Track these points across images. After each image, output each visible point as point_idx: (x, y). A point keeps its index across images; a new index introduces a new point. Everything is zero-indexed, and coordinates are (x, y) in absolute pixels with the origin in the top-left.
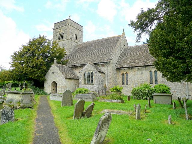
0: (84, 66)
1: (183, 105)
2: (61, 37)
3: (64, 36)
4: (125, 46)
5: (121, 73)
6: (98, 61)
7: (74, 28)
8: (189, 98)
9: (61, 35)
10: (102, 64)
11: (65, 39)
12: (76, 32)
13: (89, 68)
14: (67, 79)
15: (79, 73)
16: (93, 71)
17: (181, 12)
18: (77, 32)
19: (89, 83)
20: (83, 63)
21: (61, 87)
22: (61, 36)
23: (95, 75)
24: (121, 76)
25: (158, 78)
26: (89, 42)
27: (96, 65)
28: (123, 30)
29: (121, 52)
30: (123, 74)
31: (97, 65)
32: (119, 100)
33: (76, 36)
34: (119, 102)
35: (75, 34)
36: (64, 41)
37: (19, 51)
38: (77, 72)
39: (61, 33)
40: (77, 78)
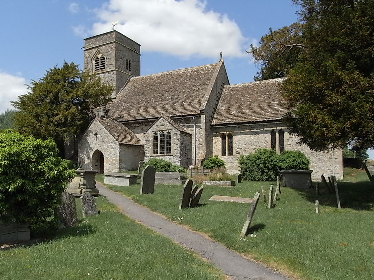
1: (274, 193)
2: (100, 63)
6: (179, 112)
7: (125, 49)
9: (100, 61)
11: (109, 70)
17: (319, 13)
19: (164, 153)
20: (150, 115)
21: (111, 160)
25: (285, 144)
28: (221, 55)
32: (229, 182)
34: (228, 184)
35: (127, 60)
37: (28, 94)
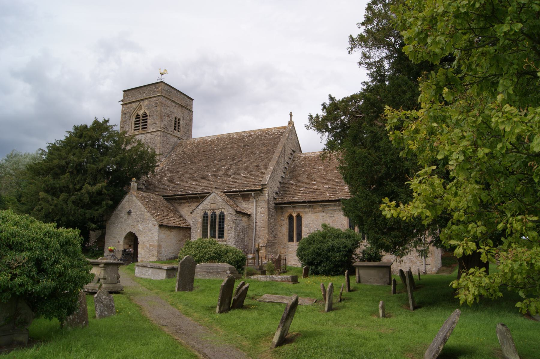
0: (205, 196)
2: (141, 121)
3: (149, 121)
4: (294, 152)
5: (287, 215)
7: (173, 104)
8: (427, 270)
9: (141, 118)
10: (246, 195)
11: (152, 130)
12: (178, 113)
13: (215, 202)
14: (163, 229)
15: (191, 213)
16: (223, 210)
18: (179, 111)
20: (199, 190)
21: (148, 246)
22: (141, 121)
23: (228, 220)
24: (286, 222)
26: (254, 131)
27: (231, 195)
28: (291, 115)
29: (286, 166)
30: (291, 218)
31: (231, 195)
33: (177, 123)
35: (175, 118)
36: (149, 135)
38: (185, 210)
39: (141, 113)
40: (182, 225)
